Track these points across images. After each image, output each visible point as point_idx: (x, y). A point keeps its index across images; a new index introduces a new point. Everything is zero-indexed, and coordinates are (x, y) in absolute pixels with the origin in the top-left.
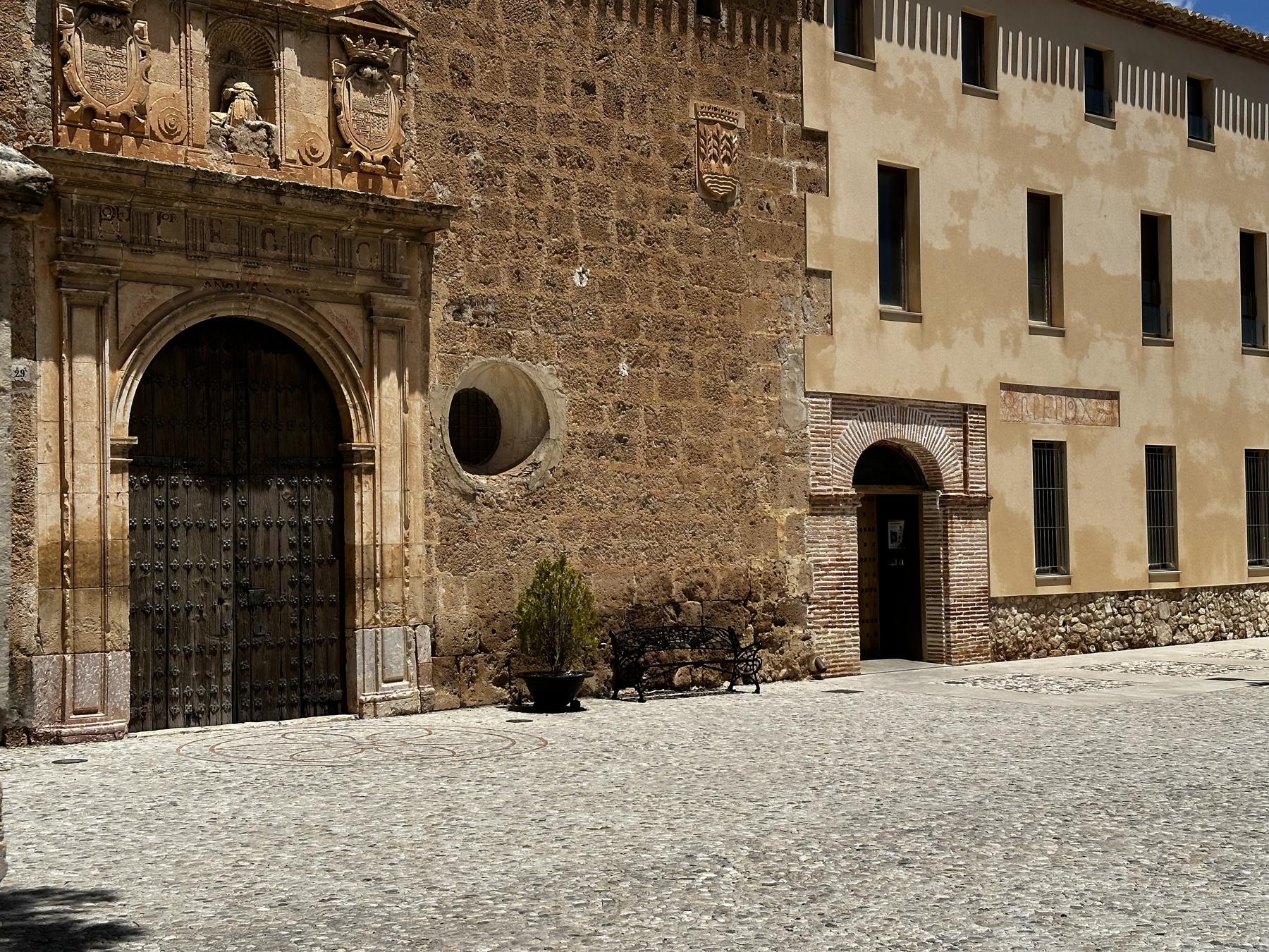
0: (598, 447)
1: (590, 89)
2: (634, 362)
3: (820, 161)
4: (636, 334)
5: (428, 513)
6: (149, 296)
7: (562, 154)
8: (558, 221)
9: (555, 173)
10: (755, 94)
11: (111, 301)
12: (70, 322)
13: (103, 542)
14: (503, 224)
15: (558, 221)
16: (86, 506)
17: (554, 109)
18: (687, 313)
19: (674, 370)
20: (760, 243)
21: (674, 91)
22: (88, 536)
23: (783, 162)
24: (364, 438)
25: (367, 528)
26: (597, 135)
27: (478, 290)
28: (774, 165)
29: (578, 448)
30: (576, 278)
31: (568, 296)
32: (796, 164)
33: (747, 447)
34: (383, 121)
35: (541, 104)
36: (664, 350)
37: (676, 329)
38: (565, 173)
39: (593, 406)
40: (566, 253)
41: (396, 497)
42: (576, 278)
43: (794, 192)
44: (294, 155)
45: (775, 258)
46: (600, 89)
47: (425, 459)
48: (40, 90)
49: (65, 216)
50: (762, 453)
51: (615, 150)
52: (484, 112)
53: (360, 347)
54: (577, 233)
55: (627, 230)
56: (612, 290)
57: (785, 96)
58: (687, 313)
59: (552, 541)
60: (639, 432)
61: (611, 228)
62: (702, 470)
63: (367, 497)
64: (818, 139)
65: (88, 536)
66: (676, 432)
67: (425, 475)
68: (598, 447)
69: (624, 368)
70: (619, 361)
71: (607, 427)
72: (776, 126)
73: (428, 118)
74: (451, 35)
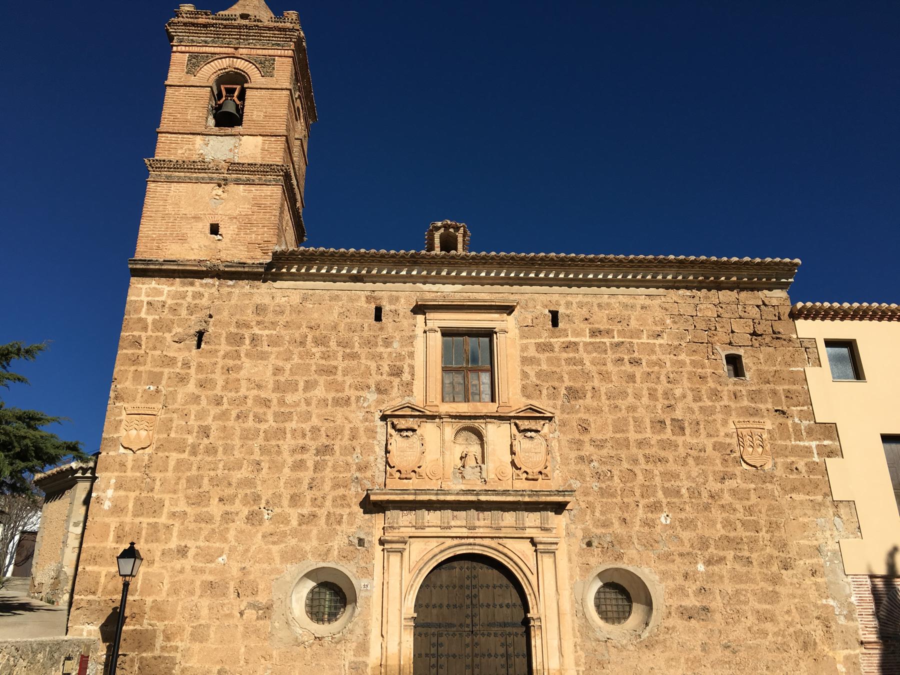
0: (688, 614)
1: (662, 422)
2: (709, 562)
3: (831, 439)
4: (708, 547)
5: (576, 652)
6: (424, 547)
7: (647, 458)
8: (647, 491)
9: (644, 466)
10: (776, 411)
11: (407, 551)
12: (388, 562)
13: (400, 665)
14: (613, 495)
15: (647, 491)
16: (393, 648)
17: (640, 437)
18: (741, 532)
19: (740, 568)
20: (794, 489)
21: (719, 417)
22: (393, 662)
23: (807, 444)
24: (536, 611)
25: (539, 660)
26: (665, 445)
27: (599, 531)
28: (798, 446)
29: (673, 614)
30: (663, 520)
31: (658, 529)
32: (814, 444)
33: (803, 611)
34: (532, 451)
35: (632, 436)
36: (730, 555)
37: (738, 544)
38: (650, 467)
39: (681, 589)
40: (655, 507)
41: (555, 643)
42: (663, 520)
43: (816, 459)
44: (493, 476)
45: (808, 497)
46: (668, 422)
47: (573, 621)
48: (381, 465)
49: (507, 587)
50: (815, 614)
51: (682, 451)
52: (599, 445)
53: (532, 564)
54: (660, 495)
55: (694, 493)
56: (688, 524)
57: (799, 408)
58: (741, 532)
59: (660, 669)
60: (717, 603)
61: (684, 491)
62: (769, 626)
63: (539, 642)
64: (830, 430)
65: (393, 662)
66: (746, 603)
67: (573, 629)
68: (688, 614)
69: (701, 567)
70: (697, 563)
71: (692, 602)
72: (795, 425)
73: (566, 450)
74: (578, 411)
